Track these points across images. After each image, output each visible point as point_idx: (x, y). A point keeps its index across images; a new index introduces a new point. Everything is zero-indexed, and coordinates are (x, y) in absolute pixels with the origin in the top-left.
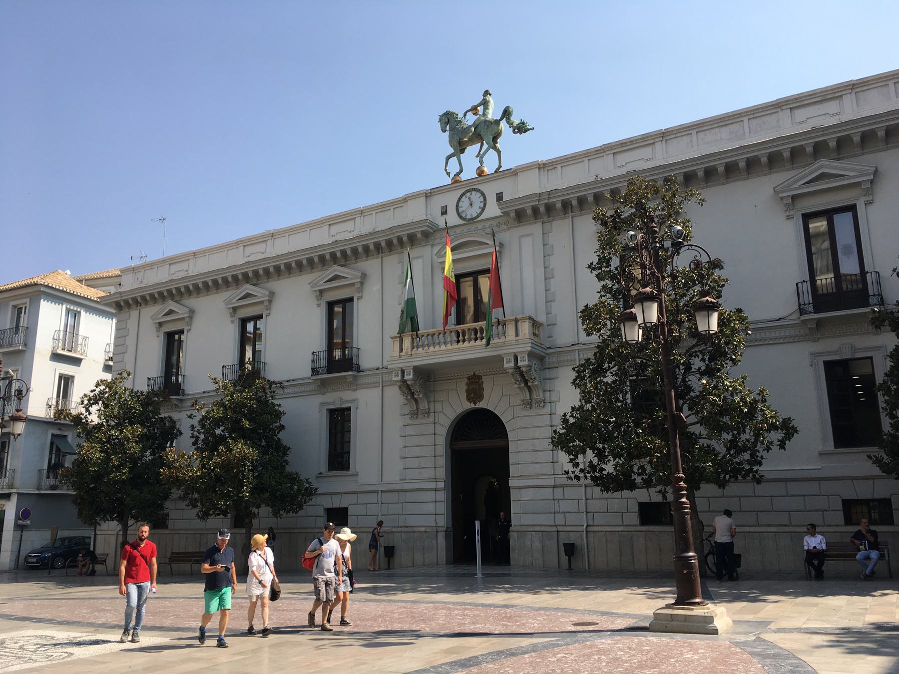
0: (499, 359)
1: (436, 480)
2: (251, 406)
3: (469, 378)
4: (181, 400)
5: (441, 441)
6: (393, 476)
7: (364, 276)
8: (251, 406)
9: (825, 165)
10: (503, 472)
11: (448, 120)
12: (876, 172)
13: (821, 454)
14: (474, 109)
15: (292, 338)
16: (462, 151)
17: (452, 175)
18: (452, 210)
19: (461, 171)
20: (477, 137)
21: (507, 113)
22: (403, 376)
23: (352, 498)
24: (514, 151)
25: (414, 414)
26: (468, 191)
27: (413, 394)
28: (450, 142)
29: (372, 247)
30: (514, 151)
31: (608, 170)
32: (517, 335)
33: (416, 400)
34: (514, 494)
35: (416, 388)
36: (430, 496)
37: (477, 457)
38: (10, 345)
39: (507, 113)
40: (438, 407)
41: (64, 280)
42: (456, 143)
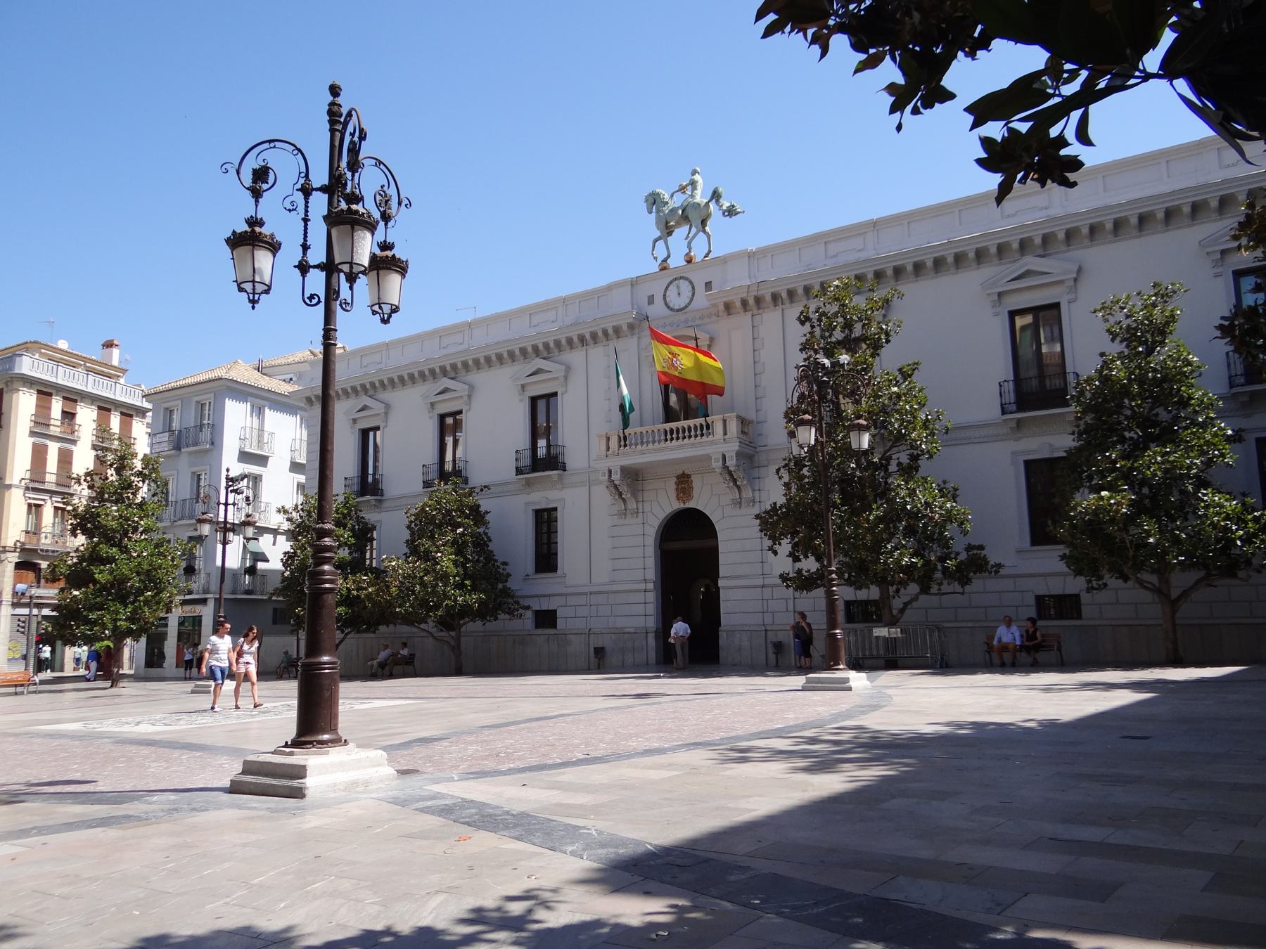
0: (707, 458)
1: (645, 581)
2: (453, 514)
3: (678, 477)
4: (380, 501)
5: (651, 541)
6: (602, 575)
7: (568, 369)
8: (453, 514)
9: (1031, 262)
10: (714, 575)
11: (654, 201)
12: (1079, 270)
13: (1019, 552)
14: (682, 189)
15: (493, 439)
16: (670, 234)
17: (659, 261)
18: (659, 300)
19: (669, 256)
20: (685, 218)
21: (716, 196)
22: (610, 476)
23: (561, 600)
24: (725, 238)
25: (623, 514)
26: (676, 279)
27: (620, 494)
28: (657, 224)
29: (576, 339)
30: (725, 238)
31: (818, 264)
32: (725, 434)
33: (624, 500)
34: (723, 595)
35: (623, 488)
36: (640, 597)
37: (687, 552)
38: (196, 444)
39: (716, 196)
40: (647, 507)
41: (244, 373)
42: (663, 226)
